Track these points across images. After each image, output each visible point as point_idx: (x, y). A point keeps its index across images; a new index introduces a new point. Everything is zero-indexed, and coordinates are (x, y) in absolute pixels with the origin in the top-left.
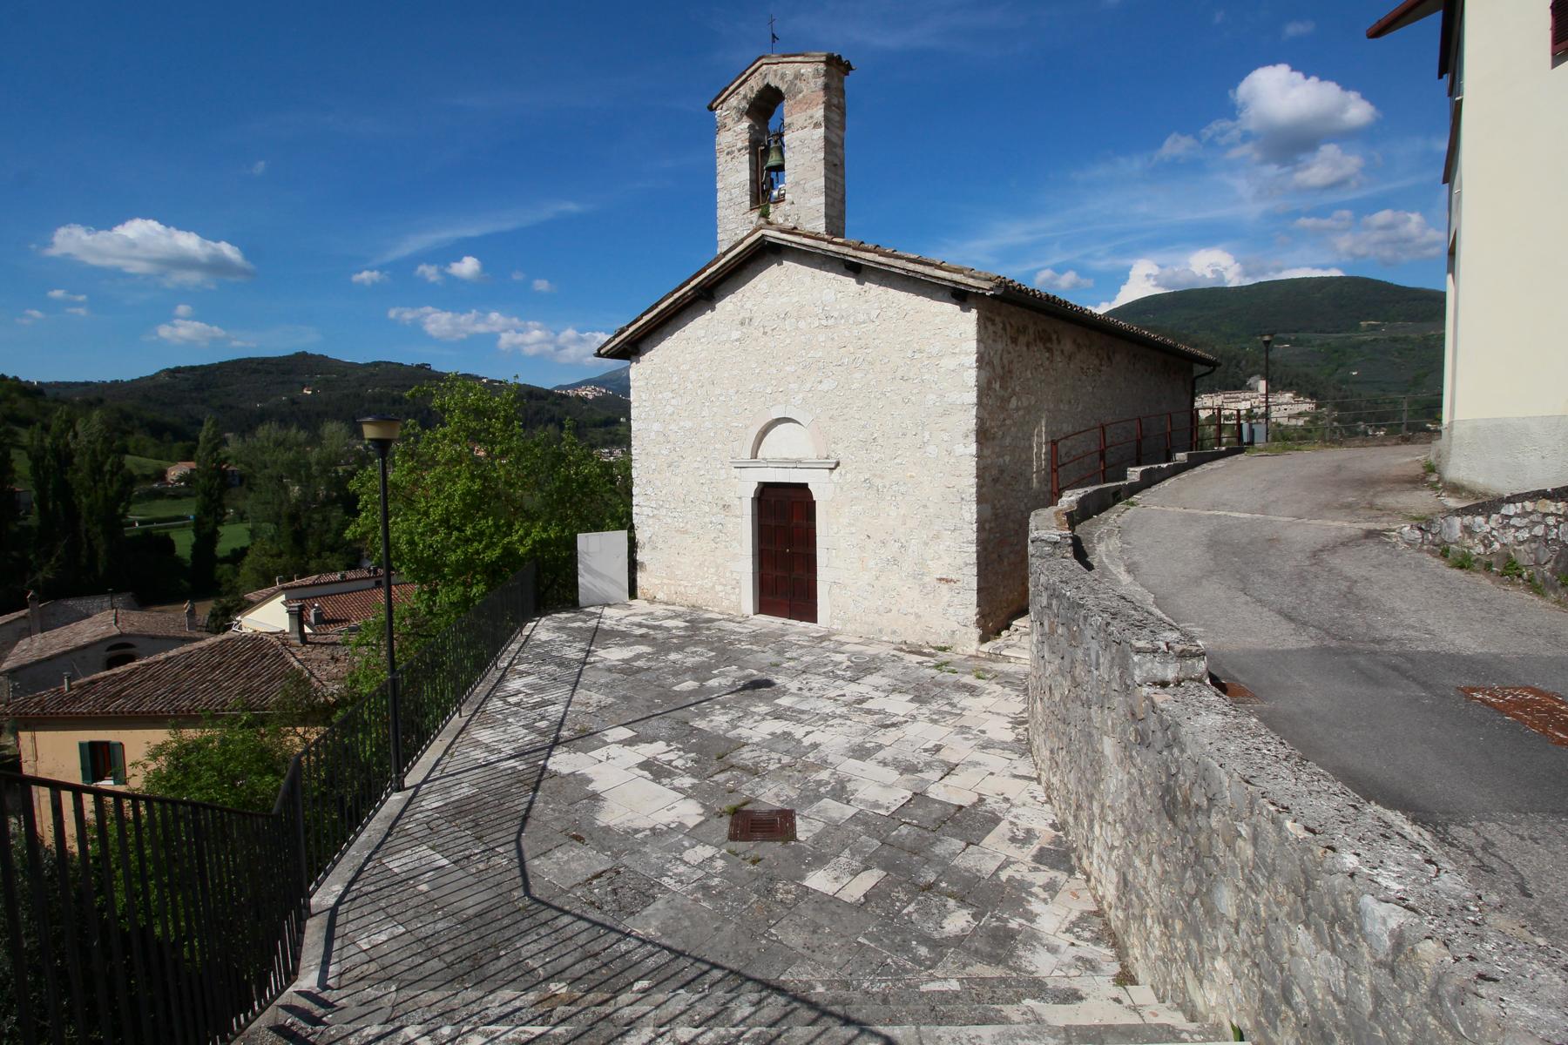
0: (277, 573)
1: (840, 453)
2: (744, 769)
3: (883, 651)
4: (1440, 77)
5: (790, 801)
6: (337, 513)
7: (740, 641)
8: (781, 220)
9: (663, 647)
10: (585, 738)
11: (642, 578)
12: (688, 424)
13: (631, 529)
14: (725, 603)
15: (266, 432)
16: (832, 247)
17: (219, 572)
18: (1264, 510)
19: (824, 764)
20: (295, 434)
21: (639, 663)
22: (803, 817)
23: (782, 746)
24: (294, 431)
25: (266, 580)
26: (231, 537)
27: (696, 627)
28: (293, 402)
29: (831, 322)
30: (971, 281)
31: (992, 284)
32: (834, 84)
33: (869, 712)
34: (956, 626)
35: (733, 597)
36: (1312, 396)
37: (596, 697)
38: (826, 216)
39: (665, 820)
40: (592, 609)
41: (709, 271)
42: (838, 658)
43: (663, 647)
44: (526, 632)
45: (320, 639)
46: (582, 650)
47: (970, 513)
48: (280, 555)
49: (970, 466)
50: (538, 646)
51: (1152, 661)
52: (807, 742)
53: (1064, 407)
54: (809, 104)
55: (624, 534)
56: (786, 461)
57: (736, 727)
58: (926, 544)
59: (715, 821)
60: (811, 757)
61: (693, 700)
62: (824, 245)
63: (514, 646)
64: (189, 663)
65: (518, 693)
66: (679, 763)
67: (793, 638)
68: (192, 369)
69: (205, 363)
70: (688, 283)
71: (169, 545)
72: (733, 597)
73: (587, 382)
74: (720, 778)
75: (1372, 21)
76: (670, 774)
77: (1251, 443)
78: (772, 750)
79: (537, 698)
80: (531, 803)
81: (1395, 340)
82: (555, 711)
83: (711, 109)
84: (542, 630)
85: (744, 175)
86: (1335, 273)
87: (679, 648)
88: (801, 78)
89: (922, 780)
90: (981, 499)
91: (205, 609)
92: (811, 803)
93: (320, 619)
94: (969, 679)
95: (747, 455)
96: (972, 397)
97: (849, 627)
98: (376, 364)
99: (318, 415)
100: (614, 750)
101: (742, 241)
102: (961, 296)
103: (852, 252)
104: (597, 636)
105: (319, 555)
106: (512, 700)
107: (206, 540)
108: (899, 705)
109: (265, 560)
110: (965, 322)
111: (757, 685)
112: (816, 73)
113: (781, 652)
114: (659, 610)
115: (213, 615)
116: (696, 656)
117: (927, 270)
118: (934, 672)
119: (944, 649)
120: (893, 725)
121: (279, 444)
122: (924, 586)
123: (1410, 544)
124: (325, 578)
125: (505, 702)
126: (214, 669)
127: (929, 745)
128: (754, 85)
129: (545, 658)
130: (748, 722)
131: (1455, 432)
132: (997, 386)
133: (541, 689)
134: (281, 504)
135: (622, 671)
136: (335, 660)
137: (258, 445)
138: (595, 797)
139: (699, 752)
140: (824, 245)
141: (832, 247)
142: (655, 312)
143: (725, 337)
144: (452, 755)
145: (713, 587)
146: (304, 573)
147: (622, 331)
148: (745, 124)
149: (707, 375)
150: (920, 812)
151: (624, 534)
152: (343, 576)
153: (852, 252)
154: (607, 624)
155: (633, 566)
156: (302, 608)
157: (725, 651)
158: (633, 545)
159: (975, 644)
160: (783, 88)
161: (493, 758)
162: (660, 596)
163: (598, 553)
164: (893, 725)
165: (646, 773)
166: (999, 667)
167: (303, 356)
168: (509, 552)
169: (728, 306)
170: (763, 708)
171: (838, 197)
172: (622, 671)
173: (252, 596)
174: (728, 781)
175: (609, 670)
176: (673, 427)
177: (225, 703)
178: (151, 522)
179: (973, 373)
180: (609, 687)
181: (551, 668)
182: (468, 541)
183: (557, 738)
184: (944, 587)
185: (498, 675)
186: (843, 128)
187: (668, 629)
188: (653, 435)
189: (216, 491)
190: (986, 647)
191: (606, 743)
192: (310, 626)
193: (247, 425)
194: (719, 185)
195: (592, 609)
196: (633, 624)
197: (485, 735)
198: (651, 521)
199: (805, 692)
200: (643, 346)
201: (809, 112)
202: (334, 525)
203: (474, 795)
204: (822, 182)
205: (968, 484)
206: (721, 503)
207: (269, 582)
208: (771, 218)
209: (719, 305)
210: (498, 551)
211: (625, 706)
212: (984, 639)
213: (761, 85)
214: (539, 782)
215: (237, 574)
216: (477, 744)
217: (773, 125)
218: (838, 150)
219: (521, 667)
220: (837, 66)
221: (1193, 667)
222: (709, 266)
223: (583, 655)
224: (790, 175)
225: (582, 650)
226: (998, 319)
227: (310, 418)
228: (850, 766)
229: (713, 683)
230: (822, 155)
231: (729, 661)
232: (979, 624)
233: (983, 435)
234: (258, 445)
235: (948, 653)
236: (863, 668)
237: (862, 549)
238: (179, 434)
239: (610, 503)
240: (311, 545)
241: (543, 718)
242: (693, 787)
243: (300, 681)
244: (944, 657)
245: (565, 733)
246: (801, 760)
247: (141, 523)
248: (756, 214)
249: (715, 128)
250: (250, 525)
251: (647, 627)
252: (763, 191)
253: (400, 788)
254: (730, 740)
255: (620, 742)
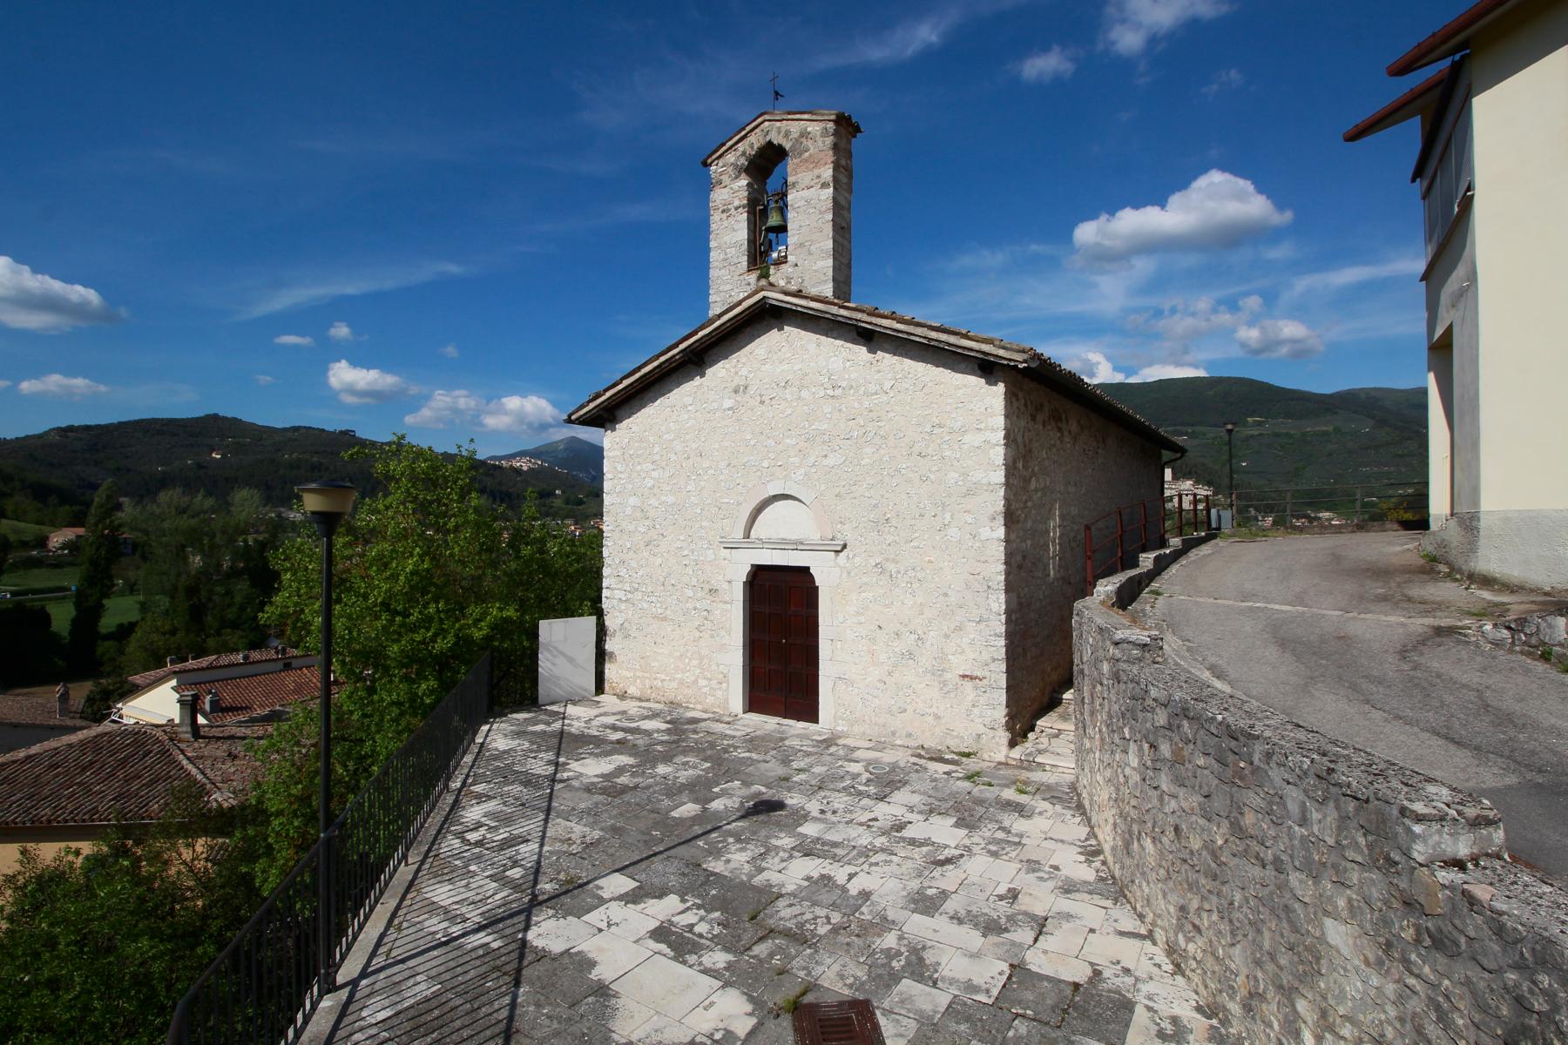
0: (168, 652)
1: (848, 534)
2: (787, 934)
3: (903, 758)
4: (1413, 180)
5: (860, 986)
6: (242, 587)
7: (736, 748)
8: (782, 283)
9: (648, 757)
10: (573, 895)
11: (610, 671)
12: (671, 499)
13: (599, 614)
14: (710, 700)
15: (169, 497)
16: (843, 312)
17: (100, 650)
18: (1299, 599)
19: (884, 924)
20: (202, 501)
21: (624, 780)
22: (888, 1012)
23: (825, 897)
24: (200, 497)
25: (156, 661)
26: (118, 610)
27: (682, 732)
28: (200, 466)
29: (838, 392)
30: (1001, 352)
31: (1025, 356)
32: (843, 144)
33: (913, 842)
34: (982, 729)
35: (719, 693)
36: (1209, 484)
37: (578, 829)
38: (834, 280)
39: (706, 1027)
40: (554, 708)
41: (701, 334)
42: (855, 768)
43: (648, 757)
44: (479, 740)
45: (215, 732)
46: (549, 763)
47: (998, 602)
48: (173, 632)
49: (998, 552)
50: (496, 758)
51: (1439, 832)
52: (854, 888)
53: (1072, 489)
54: (817, 164)
55: (591, 621)
56: (784, 541)
57: (761, 870)
58: (947, 636)
59: (771, 1024)
60: (866, 913)
61: (698, 830)
62: (834, 310)
63: (468, 759)
64: (54, 762)
65: (478, 826)
66: (702, 928)
67: (795, 743)
68: (87, 428)
69: (103, 422)
70: (676, 345)
71: (46, 619)
72: (719, 693)
73: (522, 454)
74: (761, 950)
75: (1349, 126)
76: (695, 948)
77: (1219, 529)
78: (814, 904)
79: (502, 834)
80: (513, 1005)
81: (1277, 435)
82: (528, 850)
83: (706, 165)
84: (499, 736)
85: (742, 234)
86: (1201, 373)
87: (667, 758)
88: (808, 137)
89: (1013, 943)
90: (1009, 588)
91: (81, 692)
92: (888, 987)
93: (217, 707)
94: (1009, 794)
95: (739, 534)
96: (999, 476)
97: (857, 729)
98: (296, 429)
99: (227, 480)
100: (616, 911)
101: (740, 303)
102: (987, 368)
103: (865, 317)
104: (565, 743)
105: (218, 633)
106: (473, 837)
107: (88, 615)
108: (944, 831)
109: (155, 637)
110: (991, 399)
111: (765, 808)
112: (825, 132)
113: (786, 762)
114: (632, 707)
115: (90, 700)
116: (687, 769)
117: (952, 339)
118: (967, 785)
119: (968, 755)
120: (948, 861)
121: (182, 511)
122: (945, 683)
123: (1497, 644)
124: (226, 659)
125: (464, 840)
126: (84, 769)
127: (1002, 890)
128: (755, 141)
129: (507, 775)
130: (773, 862)
131: (1483, 524)
132: (1020, 465)
133: (507, 820)
134: (179, 575)
135: (604, 791)
136: (233, 757)
137: (158, 511)
138: (602, 991)
139: (724, 910)
140: (834, 310)
141: (843, 312)
142: (637, 376)
143: (715, 405)
144: (399, 929)
145: (696, 682)
146: (200, 653)
147: (598, 396)
148: (744, 181)
149: (694, 446)
150: (1029, 996)
151: (591, 621)
152: (246, 658)
153: (865, 317)
154: (576, 727)
155: (601, 656)
156: (196, 698)
157: (723, 765)
158: (601, 632)
159: (1004, 749)
160: (787, 146)
161: (456, 930)
162: (632, 690)
163: (562, 642)
164: (948, 861)
165: (663, 947)
166: (1037, 776)
167: (214, 418)
168: (464, 641)
169: (720, 372)
170: (786, 841)
171: (845, 261)
172: (604, 791)
173: (137, 679)
174: (771, 955)
175: (589, 789)
176: (653, 501)
177: (95, 810)
178: (25, 593)
179: (1001, 450)
180: (592, 815)
181: (516, 789)
182: (414, 629)
183: (534, 896)
184: (968, 685)
185: (450, 799)
186: (851, 192)
187: (647, 733)
188: (629, 511)
189: (103, 563)
190: (1017, 753)
191: (602, 901)
192: (205, 715)
193: (147, 490)
194: (712, 244)
195: (554, 708)
196: (606, 727)
197: (442, 894)
198: (623, 606)
199: (829, 815)
200: (619, 413)
201: (816, 172)
202: (238, 599)
203: (436, 995)
204: (830, 244)
205: (996, 571)
206: (707, 587)
207: (160, 664)
208: (772, 279)
209: (710, 372)
210: (451, 639)
211: (617, 843)
212: (1012, 744)
213: (763, 142)
214: (519, 971)
215: (121, 652)
216: (433, 908)
217: (772, 184)
218: (845, 213)
219: (478, 788)
220: (846, 127)
221: (1490, 838)
222: (702, 328)
223: (551, 769)
224: (793, 237)
225: (549, 763)
226: (1021, 395)
227: (219, 484)
228: (918, 925)
229: (717, 805)
230: (830, 217)
231: (731, 775)
232: (1010, 727)
233: (1011, 518)
234: (158, 511)
235: (973, 759)
236: (887, 782)
237: (873, 640)
238: (66, 498)
239: (578, 588)
240: (216, 618)
241: (515, 864)
242: (729, 966)
243: (196, 792)
244: (972, 765)
245: (546, 887)
246: (857, 922)
247: (14, 594)
248: (753, 277)
249: (708, 185)
250: (141, 598)
251: (623, 730)
252: (761, 253)
253: (332, 987)
254: (758, 890)
255: (620, 898)
